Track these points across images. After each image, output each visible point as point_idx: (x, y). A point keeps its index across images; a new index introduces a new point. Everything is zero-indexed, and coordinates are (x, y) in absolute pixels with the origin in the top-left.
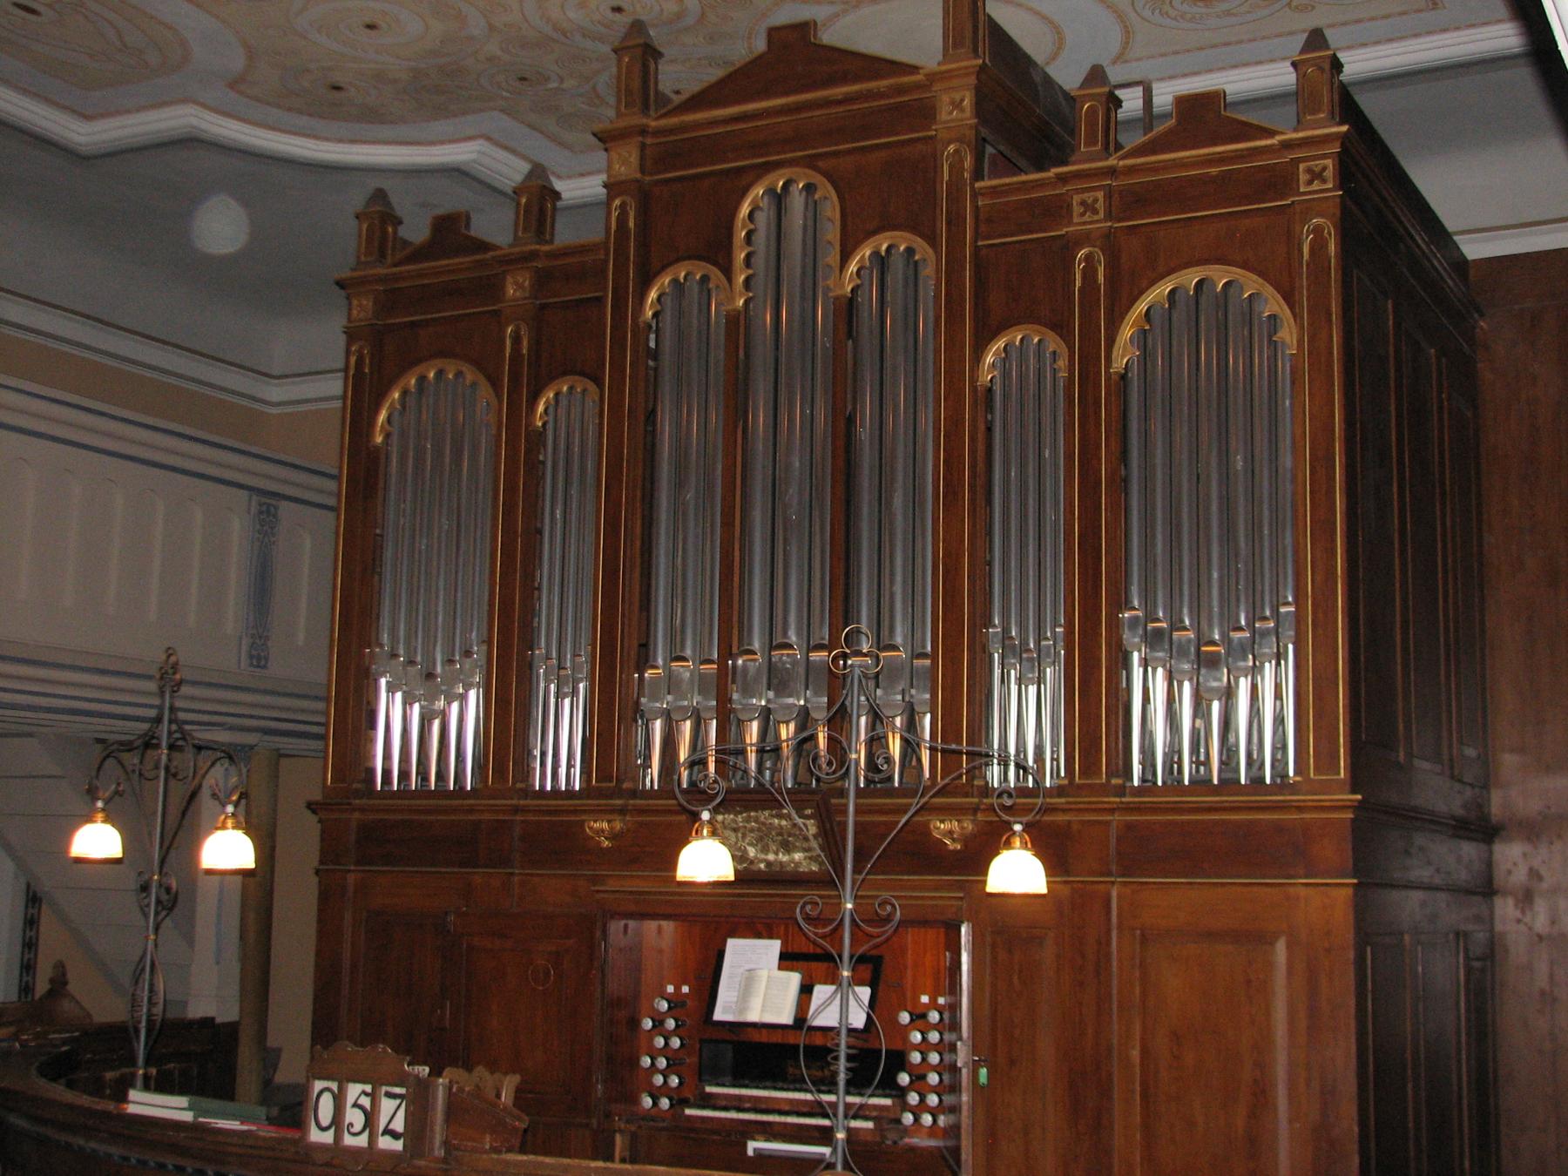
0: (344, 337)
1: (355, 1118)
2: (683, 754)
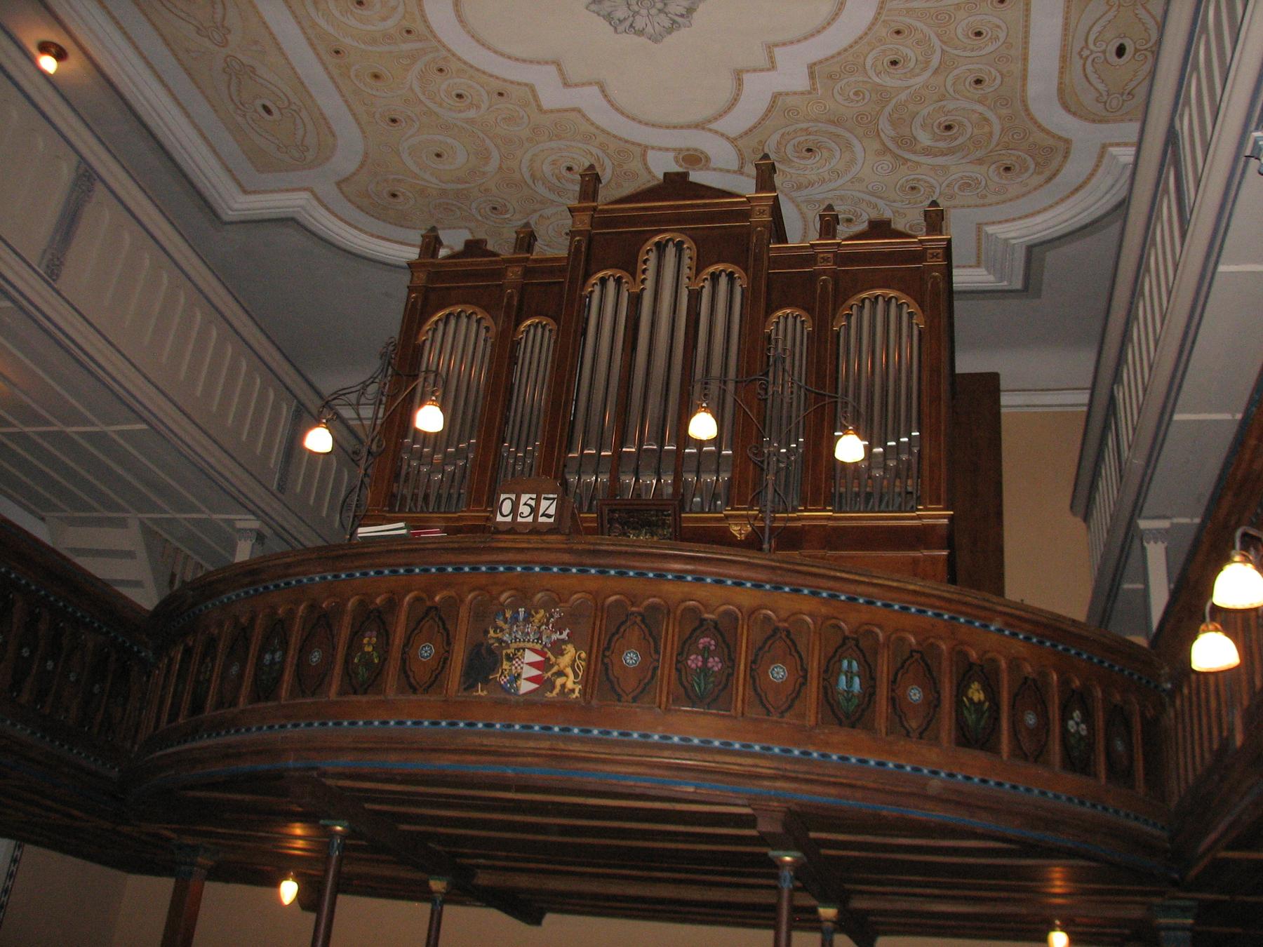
0: (407, 290)
1: (525, 510)
2: (565, 546)
